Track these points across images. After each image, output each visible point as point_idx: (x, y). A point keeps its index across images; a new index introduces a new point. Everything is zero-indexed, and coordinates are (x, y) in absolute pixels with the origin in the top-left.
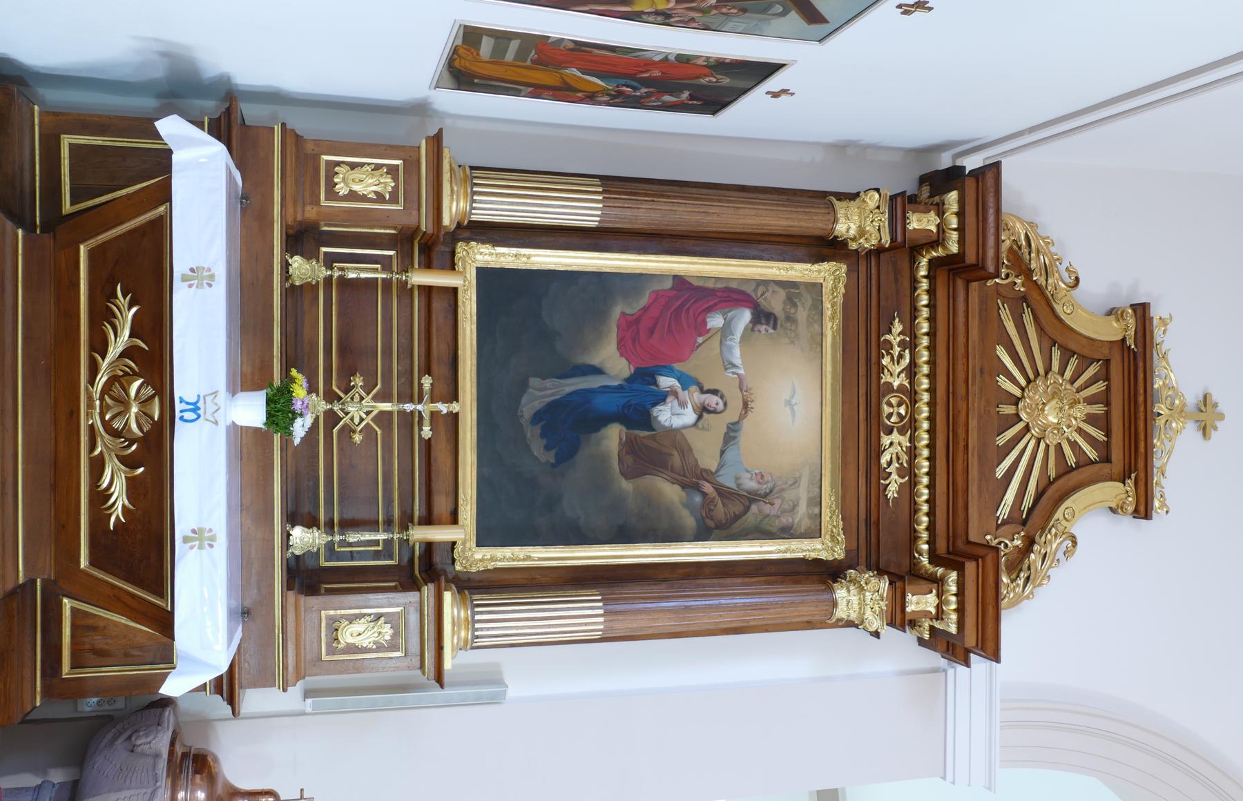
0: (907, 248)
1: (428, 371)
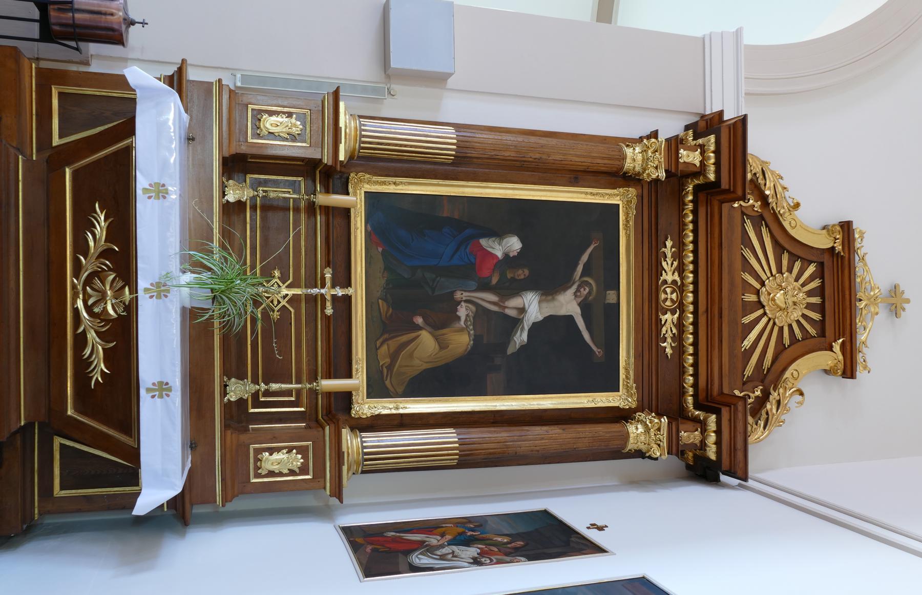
0: (678, 176)
1: (328, 264)
